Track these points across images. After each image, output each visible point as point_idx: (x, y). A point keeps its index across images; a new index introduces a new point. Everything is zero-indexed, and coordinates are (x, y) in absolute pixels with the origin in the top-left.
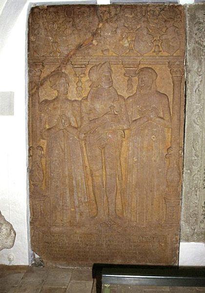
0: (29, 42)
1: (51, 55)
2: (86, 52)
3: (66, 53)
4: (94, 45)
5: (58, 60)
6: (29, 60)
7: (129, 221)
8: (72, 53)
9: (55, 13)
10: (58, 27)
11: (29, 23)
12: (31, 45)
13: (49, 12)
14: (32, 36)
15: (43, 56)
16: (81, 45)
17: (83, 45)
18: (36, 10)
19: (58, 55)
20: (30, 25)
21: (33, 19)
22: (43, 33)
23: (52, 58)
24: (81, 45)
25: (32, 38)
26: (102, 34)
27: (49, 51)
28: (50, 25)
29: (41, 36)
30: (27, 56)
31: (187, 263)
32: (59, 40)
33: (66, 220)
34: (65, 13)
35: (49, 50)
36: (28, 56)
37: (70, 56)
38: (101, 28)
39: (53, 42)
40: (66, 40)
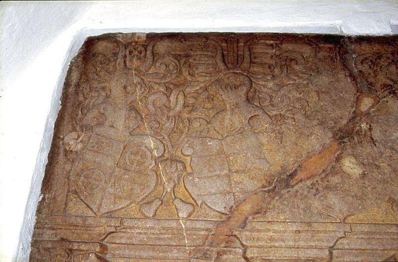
0: (56, 152)
1: (149, 212)
2: (316, 204)
3: (220, 205)
4: (349, 176)
5: (177, 233)
6: (39, 226)
7: (99, 81)
8: (247, 208)
9: (177, 57)
10: (185, 106)
11: (67, 84)
12: (62, 165)
13: (154, 54)
14: (74, 129)
15: (110, 215)
16: (292, 176)
17: (301, 175)
18: (101, 47)
19: (183, 214)
20: (71, 90)
21: (84, 74)
22: (119, 123)
23: (150, 224)
24: (292, 176)
25: (71, 140)
26: (377, 134)
27: (140, 194)
28: (152, 98)
29: (112, 132)
30: (33, 208)
31: (41, 170)
32: (189, 152)
33: (391, 48)
34: (219, 57)
35: (137, 190)
36: (39, 211)
37: (238, 218)
38: (367, 114)
39: (161, 159)
40: (220, 152)
